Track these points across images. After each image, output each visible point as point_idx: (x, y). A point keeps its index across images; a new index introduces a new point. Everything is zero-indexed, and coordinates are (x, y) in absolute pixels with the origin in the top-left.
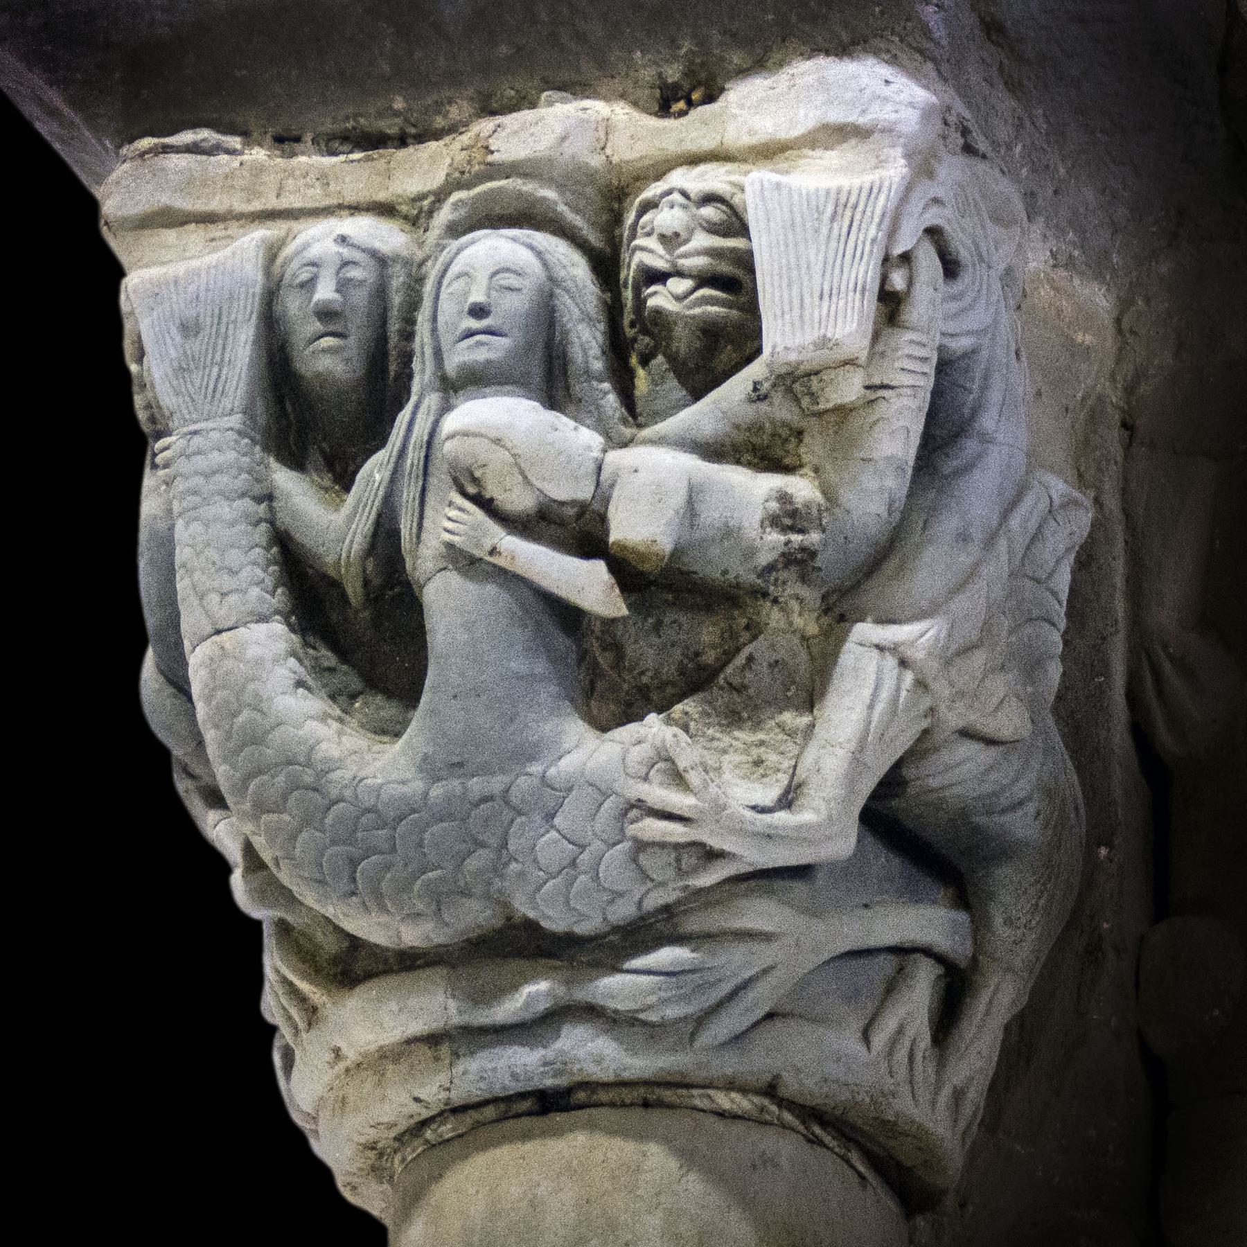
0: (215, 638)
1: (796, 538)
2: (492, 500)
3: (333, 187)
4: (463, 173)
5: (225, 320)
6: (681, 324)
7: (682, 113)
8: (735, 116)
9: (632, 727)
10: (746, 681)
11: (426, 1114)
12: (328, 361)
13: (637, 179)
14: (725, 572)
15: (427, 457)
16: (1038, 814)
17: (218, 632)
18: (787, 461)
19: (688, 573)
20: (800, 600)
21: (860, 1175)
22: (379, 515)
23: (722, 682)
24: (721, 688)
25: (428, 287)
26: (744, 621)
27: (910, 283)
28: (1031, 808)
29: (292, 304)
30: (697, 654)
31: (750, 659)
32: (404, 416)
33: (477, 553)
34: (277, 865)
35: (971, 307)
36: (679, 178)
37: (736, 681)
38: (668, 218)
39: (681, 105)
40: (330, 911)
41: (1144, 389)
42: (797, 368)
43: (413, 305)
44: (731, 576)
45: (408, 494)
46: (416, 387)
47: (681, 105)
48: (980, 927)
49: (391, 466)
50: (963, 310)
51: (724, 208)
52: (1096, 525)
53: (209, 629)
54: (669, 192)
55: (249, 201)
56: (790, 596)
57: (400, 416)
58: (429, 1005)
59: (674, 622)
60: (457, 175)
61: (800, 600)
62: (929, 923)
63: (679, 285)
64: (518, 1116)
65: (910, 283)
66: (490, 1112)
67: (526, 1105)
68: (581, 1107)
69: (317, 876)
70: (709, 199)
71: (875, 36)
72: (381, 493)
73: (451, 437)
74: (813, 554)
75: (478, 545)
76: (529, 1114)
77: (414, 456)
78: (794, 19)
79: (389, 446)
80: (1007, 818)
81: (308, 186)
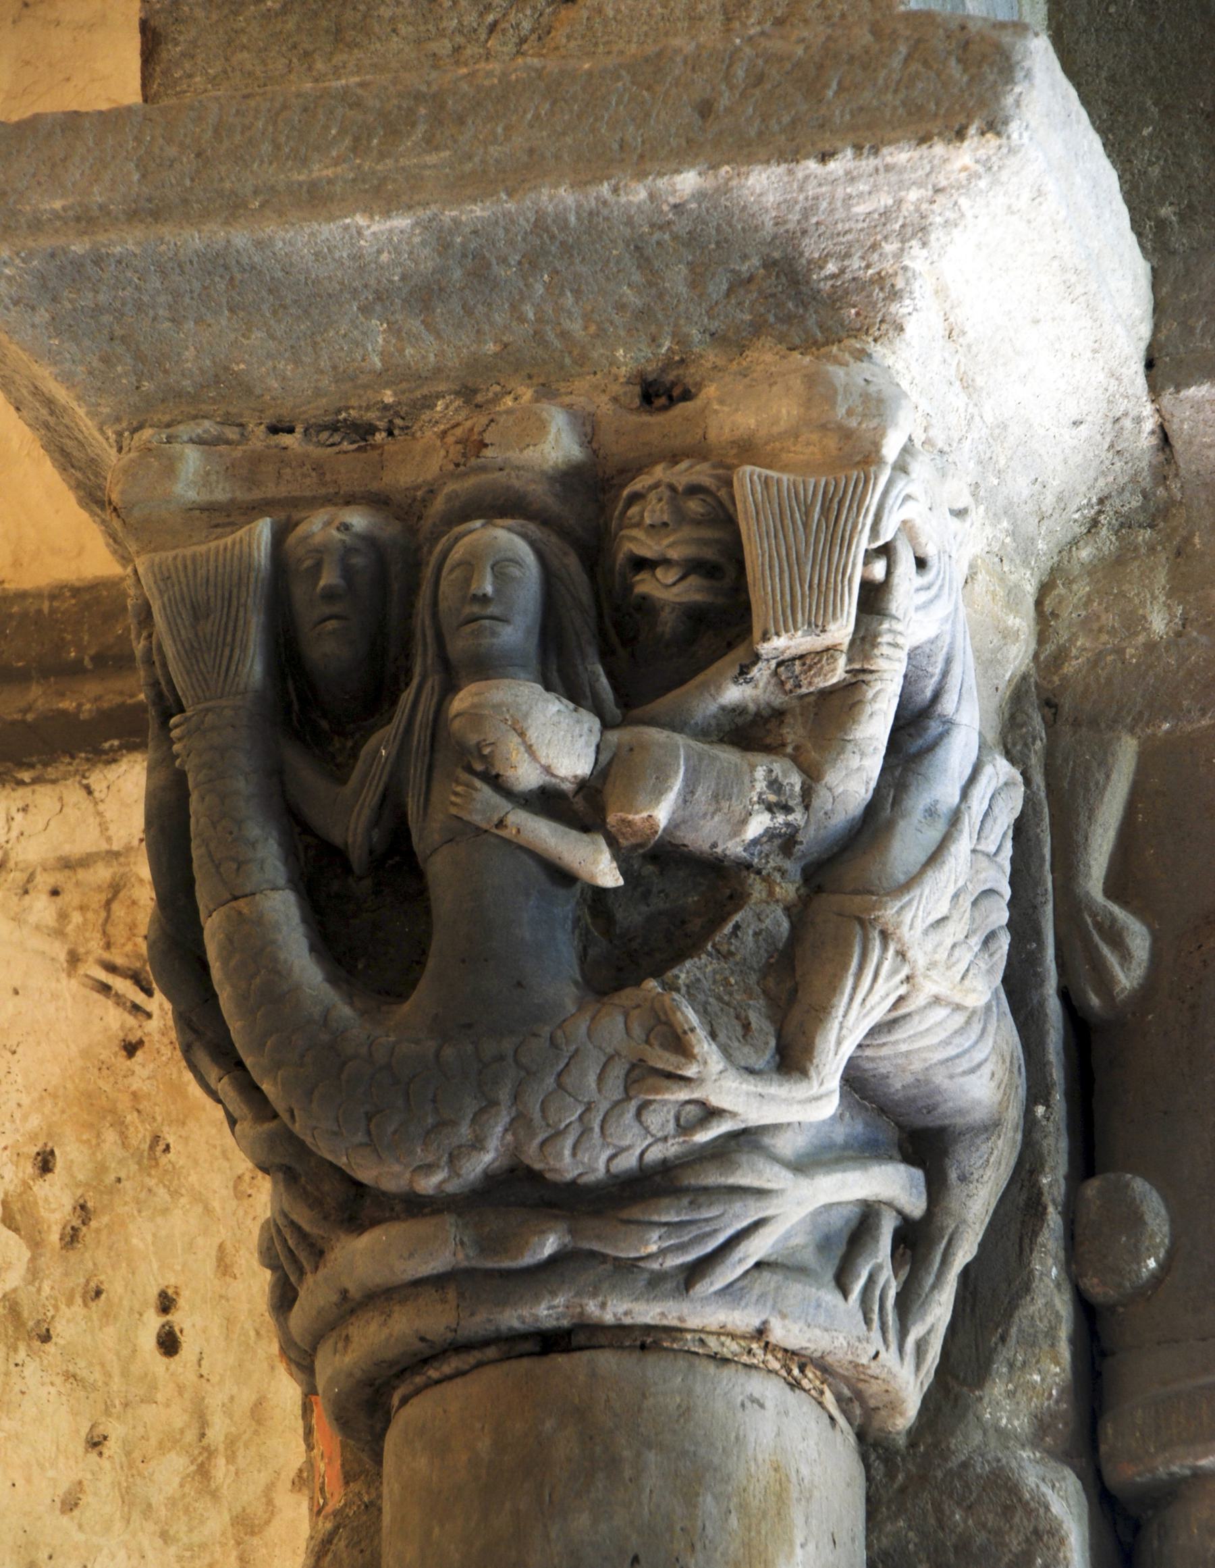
0: (234, 904)
1: (781, 818)
2: (498, 776)
3: (328, 477)
4: (457, 465)
5: (235, 603)
6: (667, 610)
7: (665, 408)
8: (716, 412)
9: (628, 992)
10: (733, 948)
11: (428, 1352)
12: (329, 647)
13: (622, 471)
14: (714, 845)
15: (433, 736)
16: (993, 1074)
17: (236, 898)
18: (768, 741)
19: (677, 846)
20: (783, 873)
21: (832, 1418)
22: (386, 789)
23: (709, 947)
24: (709, 954)
25: (428, 572)
26: (728, 892)
27: (889, 573)
28: (986, 1070)
29: (299, 592)
30: (683, 922)
31: (737, 927)
32: (407, 697)
33: (484, 825)
34: (292, 1116)
35: (937, 596)
36: (659, 472)
37: (724, 948)
38: (654, 510)
39: (663, 400)
40: (342, 1161)
41: (674, 166)
42: (783, 653)
43: (412, 589)
44: (719, 850)
45: (415, 773)
46: (417, 670)
47: (663, 400)
48: (936, 1187)
49: (397, 742)
50: (931, 601)
51: (709, 499)
52: (1028, 800)
53: (227, 896)
54: (656, 486)
55: (250, 489)
56: (774, 869)
57: (404, 696)
58: (442, 1249)
59: (662, 891)
60: (452, 467)
61: (783, 873)
62: (892, 1185)
63: (667, 576)
64: (521, 1356)
65: (889, 573)
66: (491, 1352)
67: (528, 1346)
68: (581, 1348)
69: (335, 1128)
70: (694, 490)
71: (849, 336)
72: (388, 768)
73: (458, 715)
74: (796, 830)
75: (489, 820)
76: (530, 1354)
77: (419, 735)
78: (772, 319)
79: (395, 721)
80: (962, 1080)
81: (304, 476)
